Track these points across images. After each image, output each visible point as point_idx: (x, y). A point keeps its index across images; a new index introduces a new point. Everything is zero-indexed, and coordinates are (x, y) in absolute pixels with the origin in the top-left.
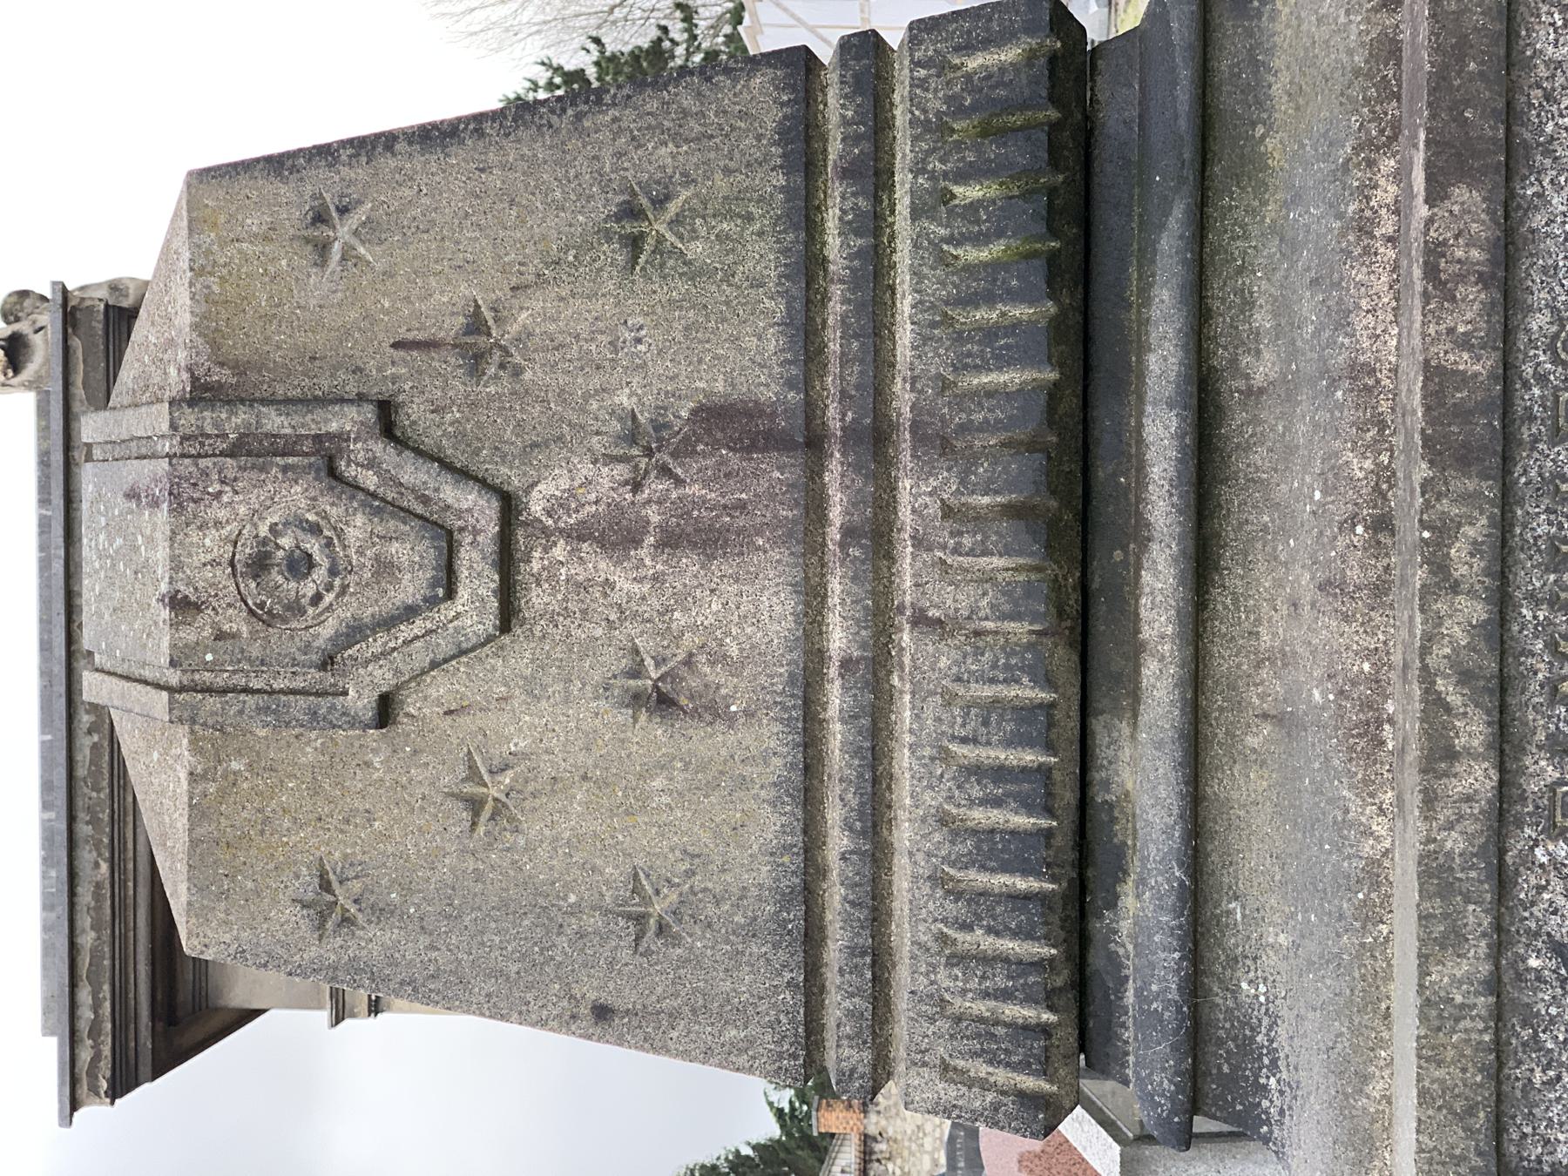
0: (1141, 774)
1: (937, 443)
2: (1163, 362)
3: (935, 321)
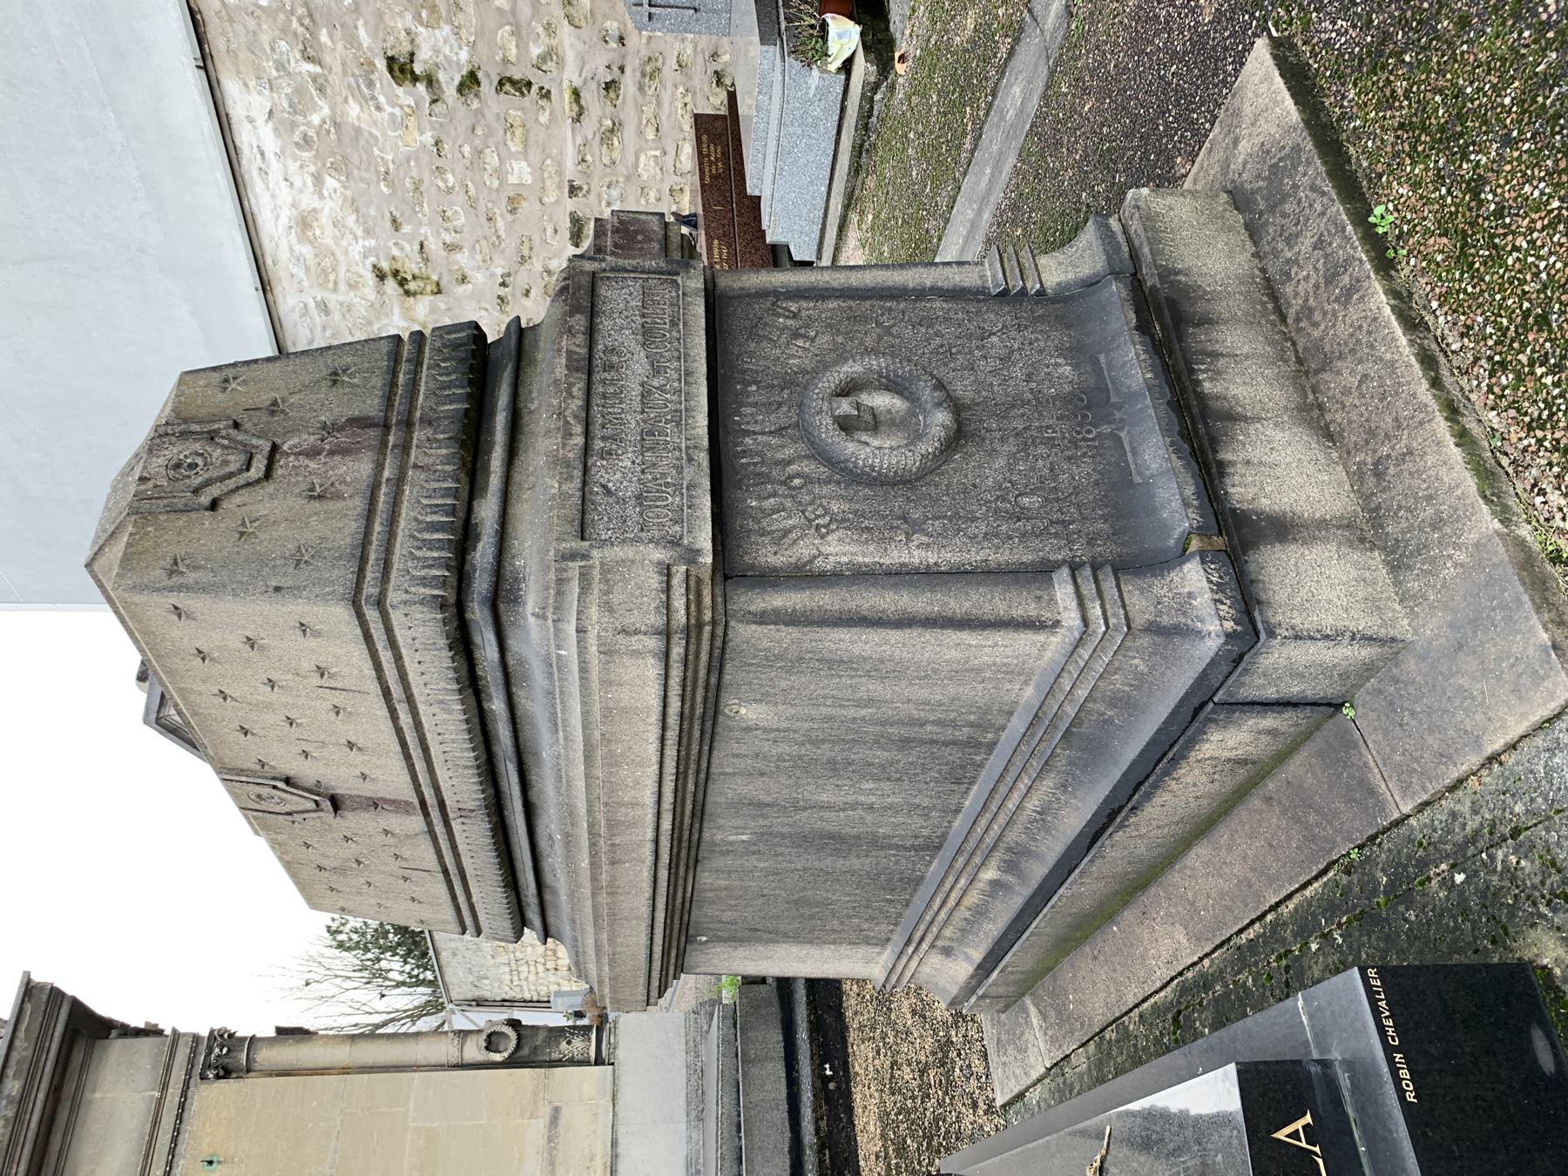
0: (487, 511)
1: (427, 422)
3: (432, 393)
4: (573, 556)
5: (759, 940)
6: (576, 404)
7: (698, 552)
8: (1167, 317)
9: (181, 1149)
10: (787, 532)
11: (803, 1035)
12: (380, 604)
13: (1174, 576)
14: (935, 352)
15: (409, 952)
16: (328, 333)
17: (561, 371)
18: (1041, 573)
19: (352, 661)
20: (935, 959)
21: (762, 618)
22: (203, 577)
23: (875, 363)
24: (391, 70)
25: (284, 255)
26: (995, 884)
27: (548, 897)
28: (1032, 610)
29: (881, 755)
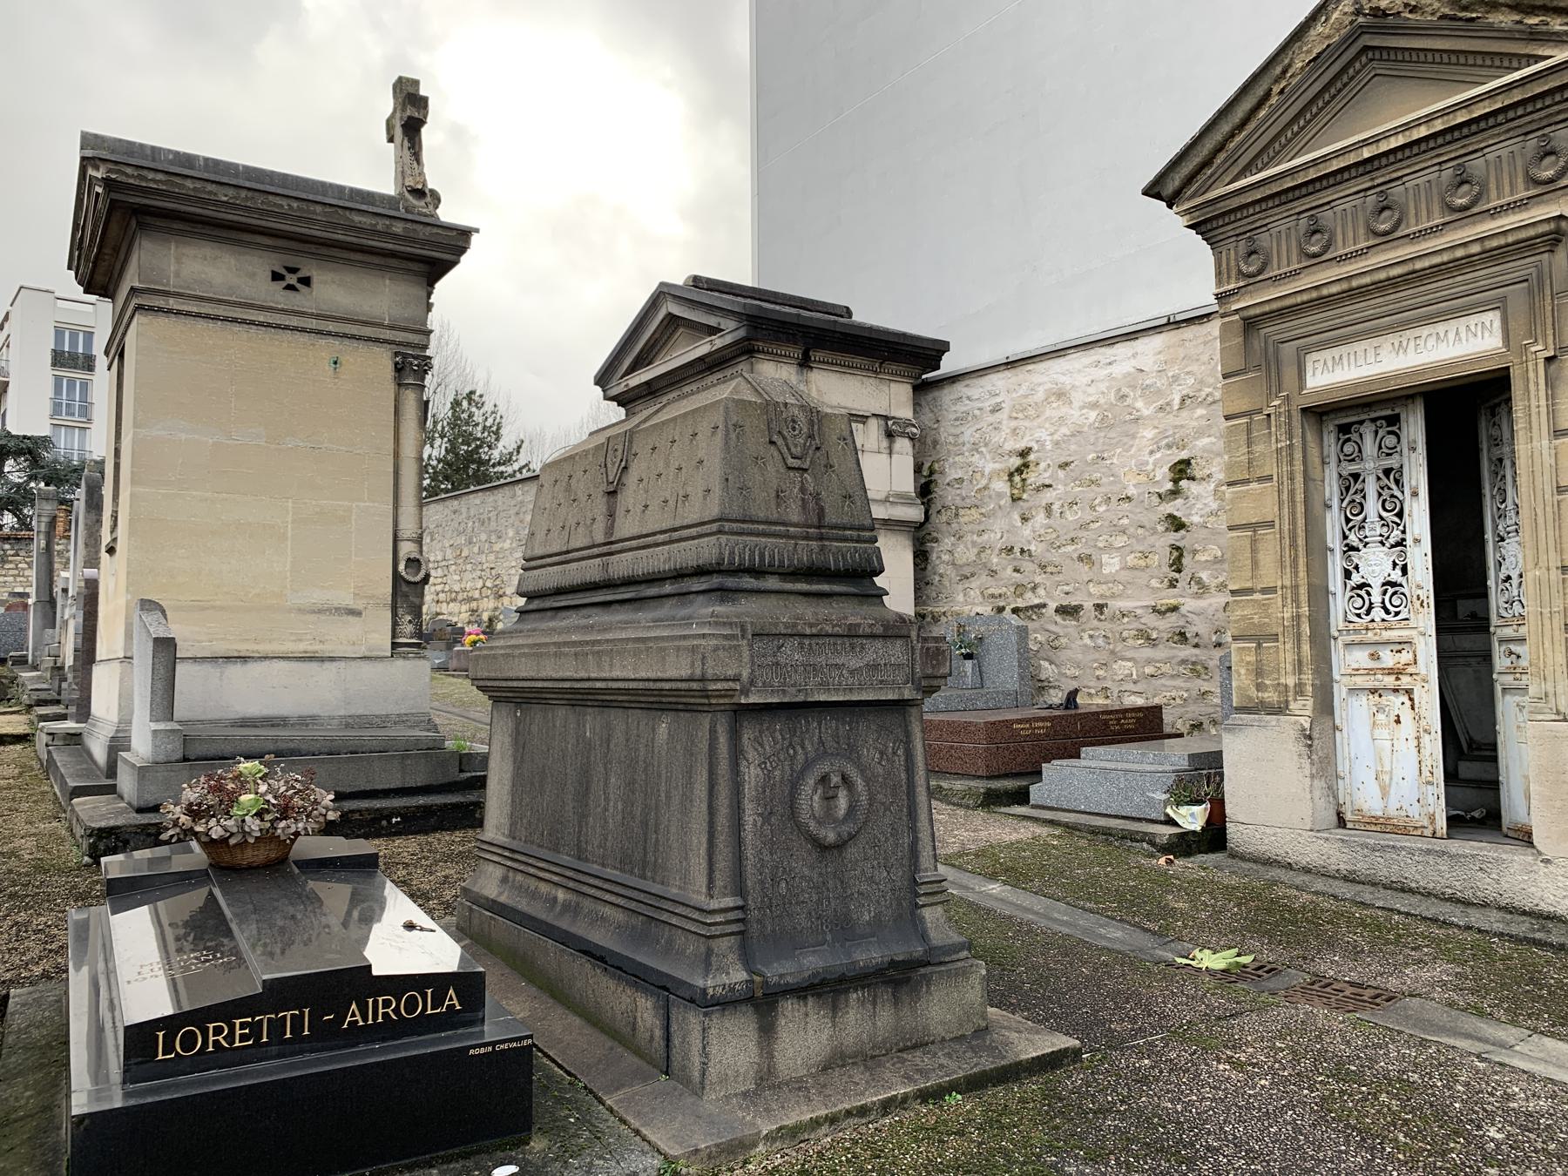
0: (772, 583)
1: (822, 548)
2: (837, 588)
4: (743, 630)
5: (516, 751)
6: (829, 629)
7: (747, 696)
8: (901, 978)
9: (347, 342)
10: (762, 745)
11: (421, 800)
12: (720, 532)
13: (739, 966)
14: (875, 837)
15: (450, 464)
16: (977, 412)
17: (852, 620)
18: (740, 890)
19: (692, 513)
20: (498, 872)
21: (713, 731)
22: (733, 443)
23: (864, 798)
24: (1181, 462)
25: (1036, 378)
26: (555, 899)
27: (549, 614)
28: (719, 883)
29: (638, 811)
